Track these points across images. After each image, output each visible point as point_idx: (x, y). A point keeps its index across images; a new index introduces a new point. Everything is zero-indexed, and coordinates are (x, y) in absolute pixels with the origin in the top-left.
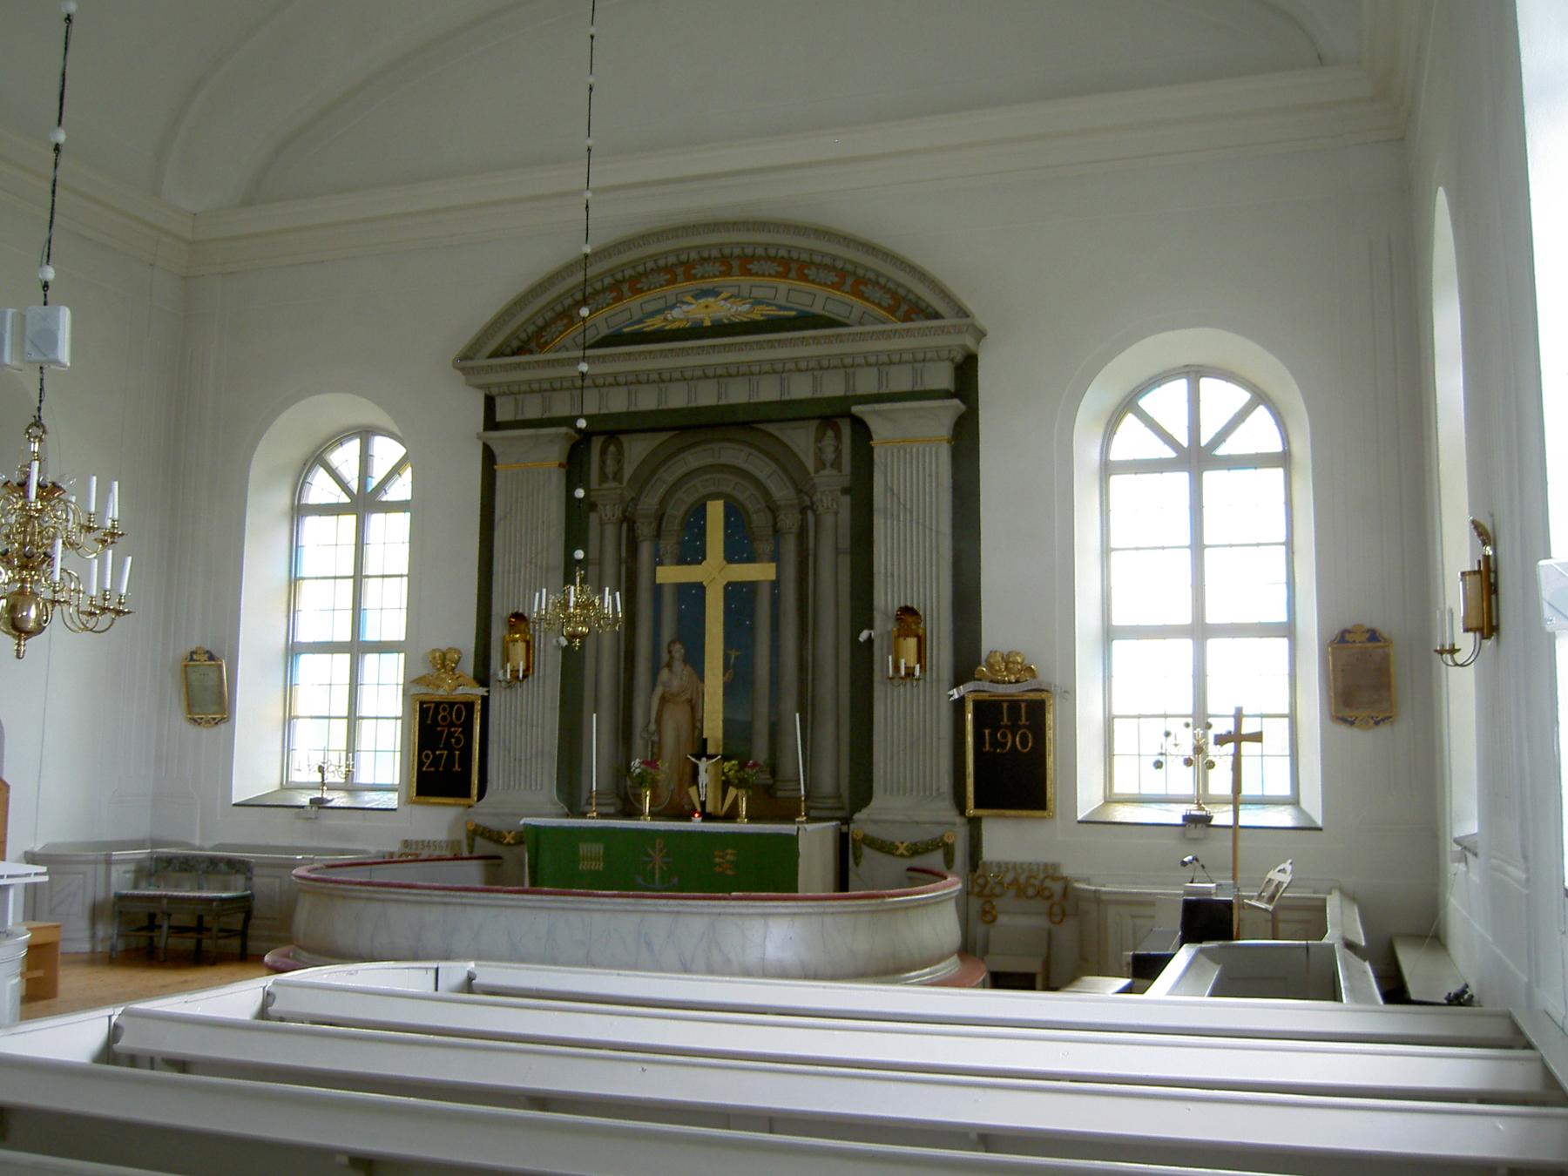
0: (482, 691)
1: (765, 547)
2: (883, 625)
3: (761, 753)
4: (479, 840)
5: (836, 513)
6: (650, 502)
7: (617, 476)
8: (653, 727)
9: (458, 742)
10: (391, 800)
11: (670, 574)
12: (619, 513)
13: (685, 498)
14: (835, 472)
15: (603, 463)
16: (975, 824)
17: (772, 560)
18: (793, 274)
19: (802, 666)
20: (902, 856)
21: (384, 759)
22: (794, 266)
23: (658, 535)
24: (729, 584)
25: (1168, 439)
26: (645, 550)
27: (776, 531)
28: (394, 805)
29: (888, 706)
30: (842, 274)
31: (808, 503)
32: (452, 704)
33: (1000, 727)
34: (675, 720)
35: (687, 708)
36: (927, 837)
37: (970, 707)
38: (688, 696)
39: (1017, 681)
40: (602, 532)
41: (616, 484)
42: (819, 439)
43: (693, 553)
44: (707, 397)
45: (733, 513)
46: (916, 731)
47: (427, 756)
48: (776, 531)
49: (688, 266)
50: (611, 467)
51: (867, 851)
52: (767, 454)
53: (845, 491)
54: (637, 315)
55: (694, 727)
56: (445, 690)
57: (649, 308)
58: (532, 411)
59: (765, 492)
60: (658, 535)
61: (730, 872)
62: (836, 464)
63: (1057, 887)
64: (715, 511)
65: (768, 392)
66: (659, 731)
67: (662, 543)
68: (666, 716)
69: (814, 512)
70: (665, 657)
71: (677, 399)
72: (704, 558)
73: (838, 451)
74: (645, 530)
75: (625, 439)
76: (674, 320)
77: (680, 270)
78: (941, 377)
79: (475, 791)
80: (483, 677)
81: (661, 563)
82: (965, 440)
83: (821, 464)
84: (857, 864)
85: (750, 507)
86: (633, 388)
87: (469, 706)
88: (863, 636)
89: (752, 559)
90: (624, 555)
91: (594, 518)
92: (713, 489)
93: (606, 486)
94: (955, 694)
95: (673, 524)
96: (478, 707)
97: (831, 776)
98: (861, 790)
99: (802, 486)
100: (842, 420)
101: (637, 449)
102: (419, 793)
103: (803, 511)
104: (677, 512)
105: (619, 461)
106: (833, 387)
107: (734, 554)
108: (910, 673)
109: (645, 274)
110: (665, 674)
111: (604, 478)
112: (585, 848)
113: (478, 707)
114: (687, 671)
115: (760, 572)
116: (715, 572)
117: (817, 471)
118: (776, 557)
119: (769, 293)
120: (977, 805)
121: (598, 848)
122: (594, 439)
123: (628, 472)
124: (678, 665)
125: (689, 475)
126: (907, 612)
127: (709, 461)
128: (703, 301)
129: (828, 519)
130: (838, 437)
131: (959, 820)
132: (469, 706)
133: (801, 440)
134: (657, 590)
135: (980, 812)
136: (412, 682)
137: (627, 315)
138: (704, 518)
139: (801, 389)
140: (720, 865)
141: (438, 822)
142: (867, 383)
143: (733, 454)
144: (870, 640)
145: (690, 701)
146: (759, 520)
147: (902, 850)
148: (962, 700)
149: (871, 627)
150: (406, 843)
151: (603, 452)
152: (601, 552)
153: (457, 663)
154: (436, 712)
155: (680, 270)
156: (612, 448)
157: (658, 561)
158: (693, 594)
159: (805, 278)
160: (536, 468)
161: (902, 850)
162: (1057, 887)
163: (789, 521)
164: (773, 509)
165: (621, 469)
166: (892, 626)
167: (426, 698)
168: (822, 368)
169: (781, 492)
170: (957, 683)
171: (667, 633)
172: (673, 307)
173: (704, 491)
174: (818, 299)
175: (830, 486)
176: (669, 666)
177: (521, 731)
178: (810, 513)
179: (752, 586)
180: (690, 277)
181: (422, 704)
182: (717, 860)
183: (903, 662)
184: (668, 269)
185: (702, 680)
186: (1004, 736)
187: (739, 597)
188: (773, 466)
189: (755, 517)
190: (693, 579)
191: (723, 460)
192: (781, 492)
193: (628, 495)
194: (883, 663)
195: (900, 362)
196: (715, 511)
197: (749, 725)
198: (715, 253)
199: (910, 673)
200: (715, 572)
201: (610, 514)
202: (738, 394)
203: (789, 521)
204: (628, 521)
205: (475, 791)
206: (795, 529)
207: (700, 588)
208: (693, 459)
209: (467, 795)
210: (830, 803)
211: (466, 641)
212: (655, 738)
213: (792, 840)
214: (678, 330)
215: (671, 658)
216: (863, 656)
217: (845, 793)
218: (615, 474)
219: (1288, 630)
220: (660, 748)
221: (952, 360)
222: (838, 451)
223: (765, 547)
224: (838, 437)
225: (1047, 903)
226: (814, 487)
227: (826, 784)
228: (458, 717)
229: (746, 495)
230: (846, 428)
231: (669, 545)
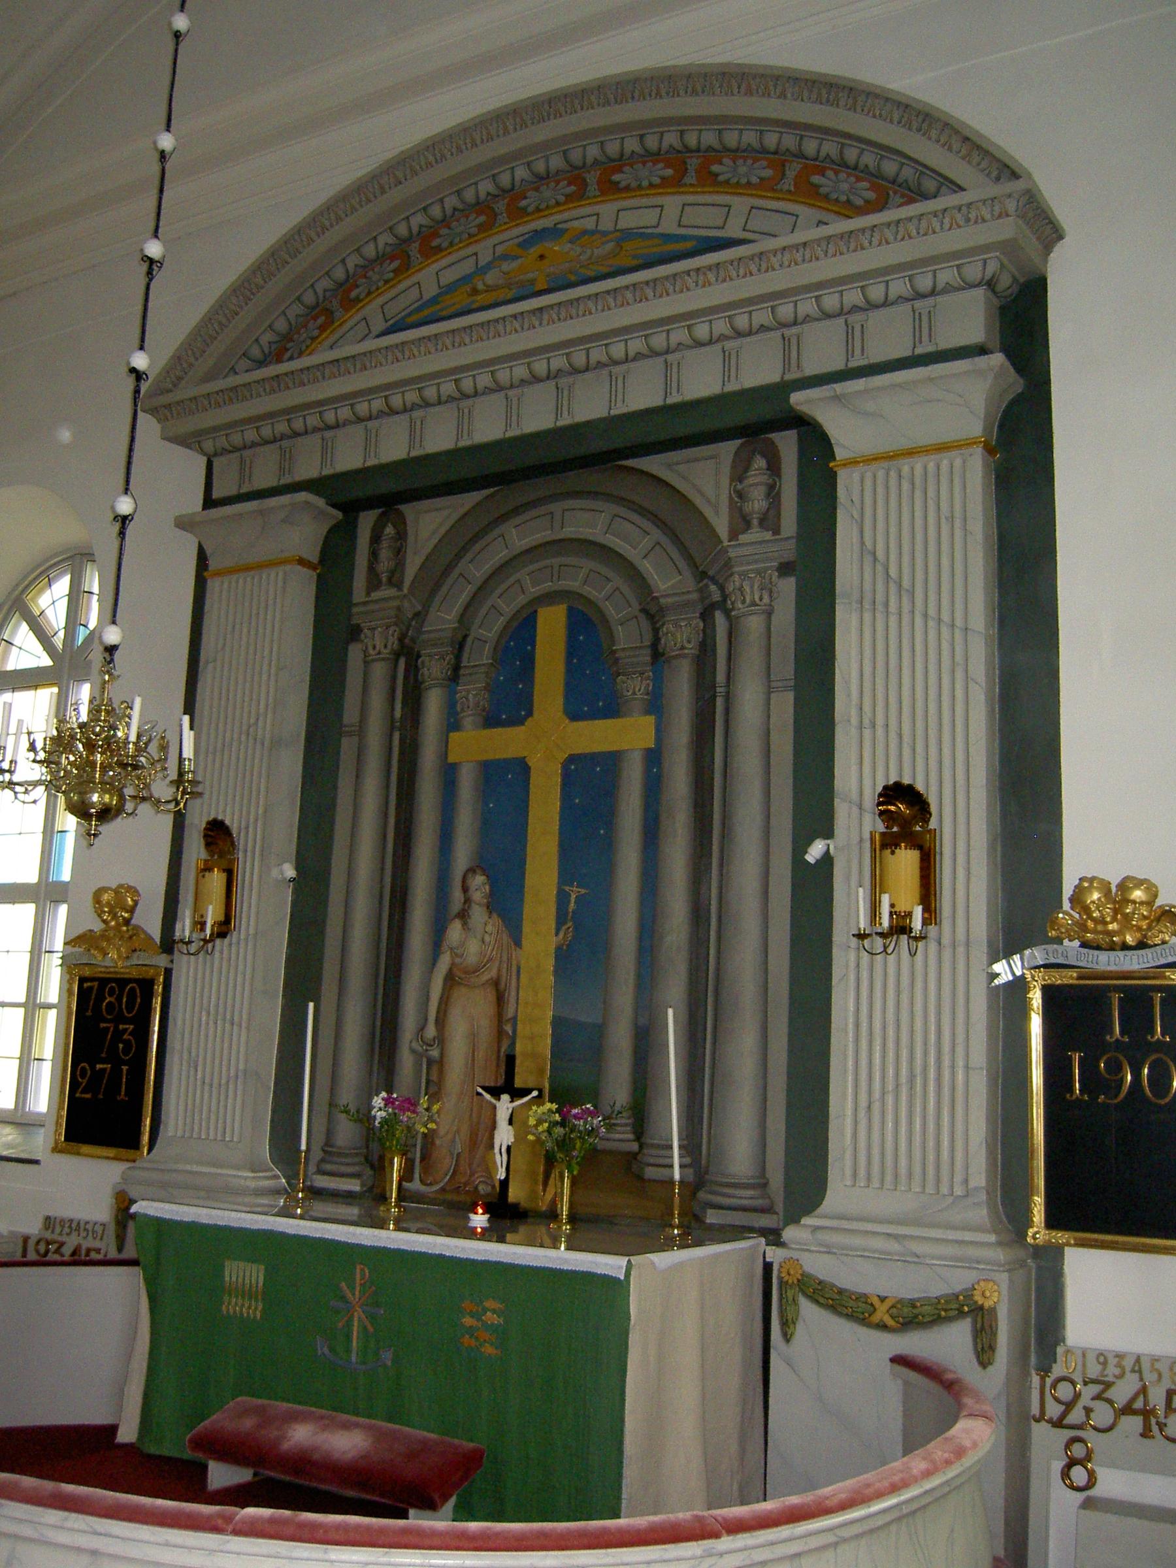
0: (162, 961)
2: (856, 820)
3: (618, 1089)
5: (769, 614)
6: (444, 618)
7: (395, 580)
8: (431, 1031)
9: (126, 1051)
11: (475, 744)
12: (393, 643)
13: (506, 604)
14: (768, 535)
15: (374, 555)
17: (648, 712)
18: (690, 179)
19: (698, 914)
20: (883, 1327)
22: (693, 163)
23: (455, 675)
24: (572, 759)
26: (433, 704)
27: (657, 654)
29: (860, 987)
30: (778, 159)
31: (716, 597)
32: (122, 982)
33: (1103, 1047)
34: (470, 1017)
35: (491, 996)
36: (937, 1289)
37: (1036, 998)
38: (493, 973)
39: (1142, 945)
41: (392, 592)
42: (740, 472)
43: (510, 705)
44: (537, 415)
45: (585, 625)
47: (83, 1075)
48: (657, 654)
49: (512, 194)
50: (385, 564)
51: (808, 1309)
52: (643, 511)
53: (785, 569)
55: (500, 1032)
57: (449, 277)
60: (455, 675)
61: (489, 1349)
64: (552, 625)
65: (643, 392)
66: (441, 1040)
69: (727, 613)
70: (457, 895)
71: (488, 426)
72: (530, 713)
73: (773, 494)
74: (433, 668)
75: (406, 509)
77: (501, 206)
78: (968, 319)
79: (145, 1138)
82: (1021, 449)
83: (740, 523)
84: (787, 1337)
85: (610, 610)
86: (417, 414)
87: (147, 985)
88: (815, 851)
90: (398, 714)
91: (355, 653)
92: (548, 586)
93: (375, 595)
94: (1004, 971)
95: (480, 657)
97: (745, 1140)
100: (764, 423)
101: (429, 522)
103: (706, 615)
104: (488, 630)
105: (399, 552)
106: (759, 369)
108: (900, 927)
109: (445, 222)
110: (455, 932)
111: (374, 583)
115: (630, 734)
117: (733, 535)
118: (655, 705)
120: (1052, 1223)
121: (252, 1274)
122: (362, 515)
123: (411, 571)
124: (478, 915)
126: (897, 792)
128: (535, 251)
129: (754, 624)
132: (147, 985)
133: (704, 477)
135: (1060, 1237)
137: (414, 294)
138: (532, 641)
139: (701, 380)
140: (471, 1331)
141: (86, 1187)
142: (822, 350)
143: (587, 520)
144: (827, 860)
145: (496, 983)
146: (628, 637)
147: (881, 1314)
148: (1019, 986)
149: (829, 834)
150: (49, 1222)
151: (376, 538)
153: (132, 911)
154: (100, 998)
155: (501, 206)
156: (389, 530)
158: (507, 780)
161: (881, 1314)
163: (681, 635)
164: (653, 613)
165: (400, 565)
166: (873, 824)
167: (87, 972)
168: (739, 334)
169: (668, 580)
173: (534, 591)
175: (755, 556)
176: (463, 915)
177: (219, 1033)
178: (719, 618)
179: (611, 762)
180: (518, 214)
181: (82, 981)
182: (468, 1321)
183: (886, 900)
184: (482, 207)
185: (518, 943)
186: (1116, 1068)
187: (590, 780)
188: (656, 534)
189: (619, 631)
190: (509, 754)
191: (569, 532)
192: (668, 580)
193: (411, 607)
194: (852, 906)
195: (886, 304)
196: (552, 625)
197: (599, 1032)
198: (557, 162)
199: (900, 927)
200: (549, 739)
201: (379, 644)
202: (590, 404)
204: (407, 653)
205: (145, 1138)
206: (691, 649)
207: (522, 768)
208: (518, 536)
209: (135, 1144)
210: (746, 1197)
212: (435, 1053)
213: (612, 1290)
215: (467, 901)
216: (814, 888)
217: (776, 1179)
218: (392, 573)
220: (441, 1071)
221: (991, 284)
223: (635, 687)
224: (774, 468)
226: (728, 565)
227: (738, 1153)
228: (130, 1008)
229: (579, 577)
230: (787, 443)
231: (472, 691)
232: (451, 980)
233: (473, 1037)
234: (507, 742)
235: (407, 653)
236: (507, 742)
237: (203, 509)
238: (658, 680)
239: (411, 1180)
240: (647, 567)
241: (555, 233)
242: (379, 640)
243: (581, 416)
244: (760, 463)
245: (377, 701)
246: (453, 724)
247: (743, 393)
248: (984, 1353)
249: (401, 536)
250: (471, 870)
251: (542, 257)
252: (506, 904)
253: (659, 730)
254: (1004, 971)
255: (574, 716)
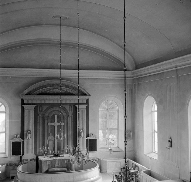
0: (22, 140)
1: (63, 121)
4: (24, 161)
6: (46, 115)
7: (42, 111)
11: (49, 124)
15: (40, 109)
23: (48, 119)
26: (46, 121)
27: (64, 119)
40: (40, 119)
45: (58, 117)
48: (64, 119)
50: (41, 110)
53: (72, 114)
54: (46, 90)
58: (30, 102)
60: (48, 119)
62: (71, 111)
64: (56, 116)
76: (51, 91)
78: (85, 102)
81: (63, 125)
83: (69, 111)
91: (38, 116)
94: (87, 138)
96: (22, 143)
102: (13, 155)
105: (42, 109)
107: (58, 122)
110: (49, 137)
111: (40, 111)
113: (22, 143)
114: (52, 136)
118: (64, 122)
124: (51, 136)
125: (57, 111)
130: (72, 107)
134: (48, 126)
135: (89, 152)
146: (62, 118)
148: (87, 139)
151: (40, 108)
157: (48, 122)
159: (68, 88)
160: (30, 111)
162: (97, 160)
163: (65, 117)
164: (63, 116)
169: (65, 114)
170: (87, 137)
171: (49, 131)
172: (51, 90)
174: (71, 91)
175: (71, 114)
176: (50, 136)
196: (56, 116)
203: (65, 117)
204: (43, 117)
208: (52, 109)
214: (48, 93)
222: (72, 109)
224: (72, 107)
232: (49, 140)
233: (51, 144)
235: (43, 117)
236: (53, 124)
237: (88, 99)
238: (64, 120)
239: (23, 141)
243: (55, 103)
244: (71, 107)
247: (58, 103)
249: (42, 108)
250: (50, 133)
254: (87, 138)
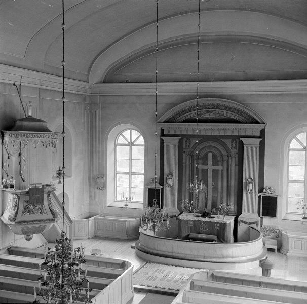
0: (162, 187)
10: (141, 206)
11: (201, 167)
16: (262, 218)
19: (228, 186)
21: (139, 197)
25: (127, 141)
26: (195, 161)
27: (223, 160)
28: (142, 208)
42: (232, 142)
45: (214, 156)
46: (251, 201)
48: (223, 160)
50: (188, 144)
53: (237, 153)
56: (153, 187)
59: (220, 152)
62: (235, 148)
63: (278, 231)
64: (210, 155)
67: (199, 161)
68: (200, 194)
78: (258, 134)
80: (162, 184)
83: (232, 148)
89: (218, 165)
94: (259, 194)
98: (239, 211)
99: (228, 152)
104: (202, 154)
112: (189, 222)
115: (220, 168)
116: (210, 167)
118: (222, 165)
119: (223, 113)
127: (209, 145)
131: (259, 218)
135: (264, 217)
136: (146, 183)
146: (219, 158)
148: (260, 195)
151: (186, 142)
152: (186, 161)
158: (205, 172)
162: (278, 231)
163: (225, 158)
164: (222, 156)
169: (224, 153)
170: (259, 193)
175: (234, 152)
187: (215, 172)
190: (217, 169)
192: (224, 153)
196: (210, 155)
200: (210, 167)
203: (225, 158)
208: (205, 144)
211: (158, 176)
219: (288, 182)
223: (220, 163)
225: (275, 234)
229: (216, 153)
231: (200, 161)
233: (202, 197)
234: (205, 167)
236: (205, 167)
240: (222, 151)
241: (211, 112)
242: (188, 153)
245: (188, 160)
246: (206, 193)
248: (257, 226)
251: (298, 209)
252: (206, 183)
253: (223, 168)
255: (213, 165)
